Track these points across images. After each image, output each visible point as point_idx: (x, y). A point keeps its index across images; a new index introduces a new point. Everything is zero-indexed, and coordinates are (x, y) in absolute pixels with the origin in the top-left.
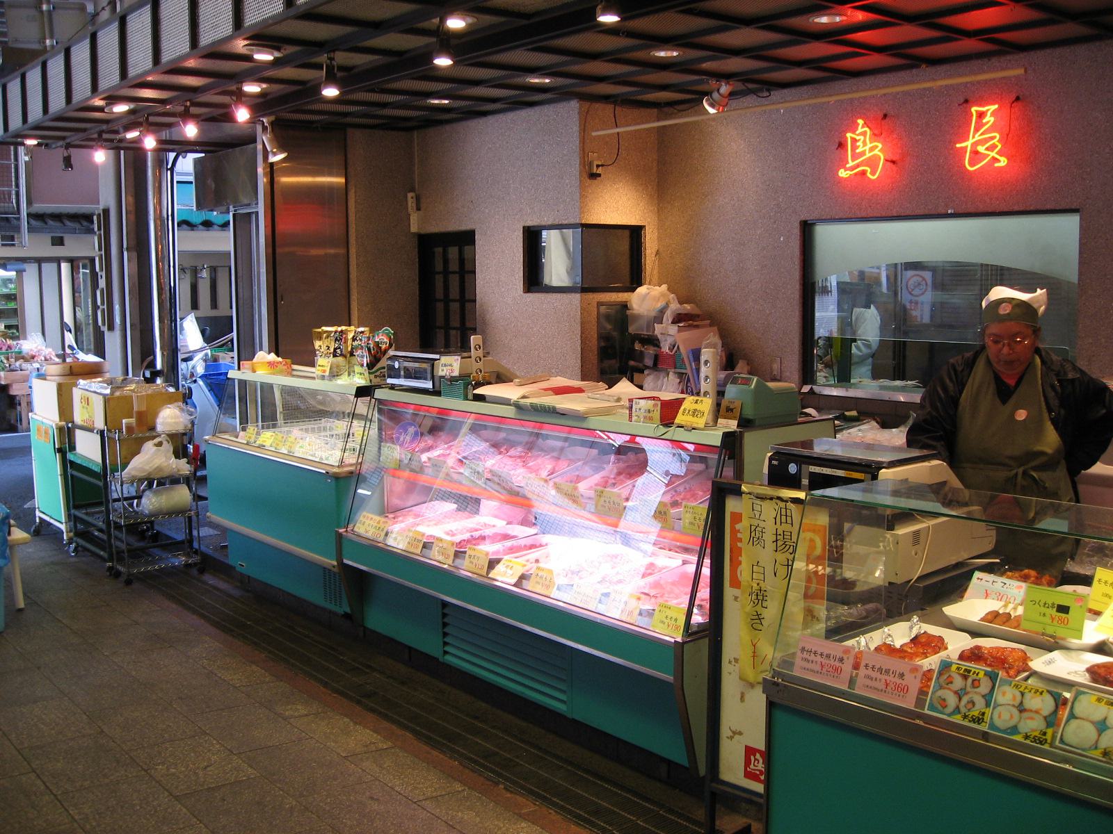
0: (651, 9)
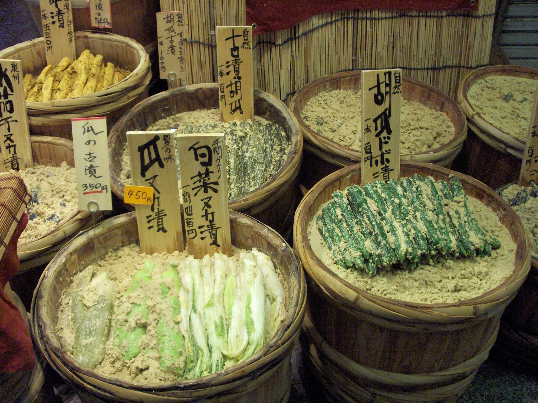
0: (60, 373)
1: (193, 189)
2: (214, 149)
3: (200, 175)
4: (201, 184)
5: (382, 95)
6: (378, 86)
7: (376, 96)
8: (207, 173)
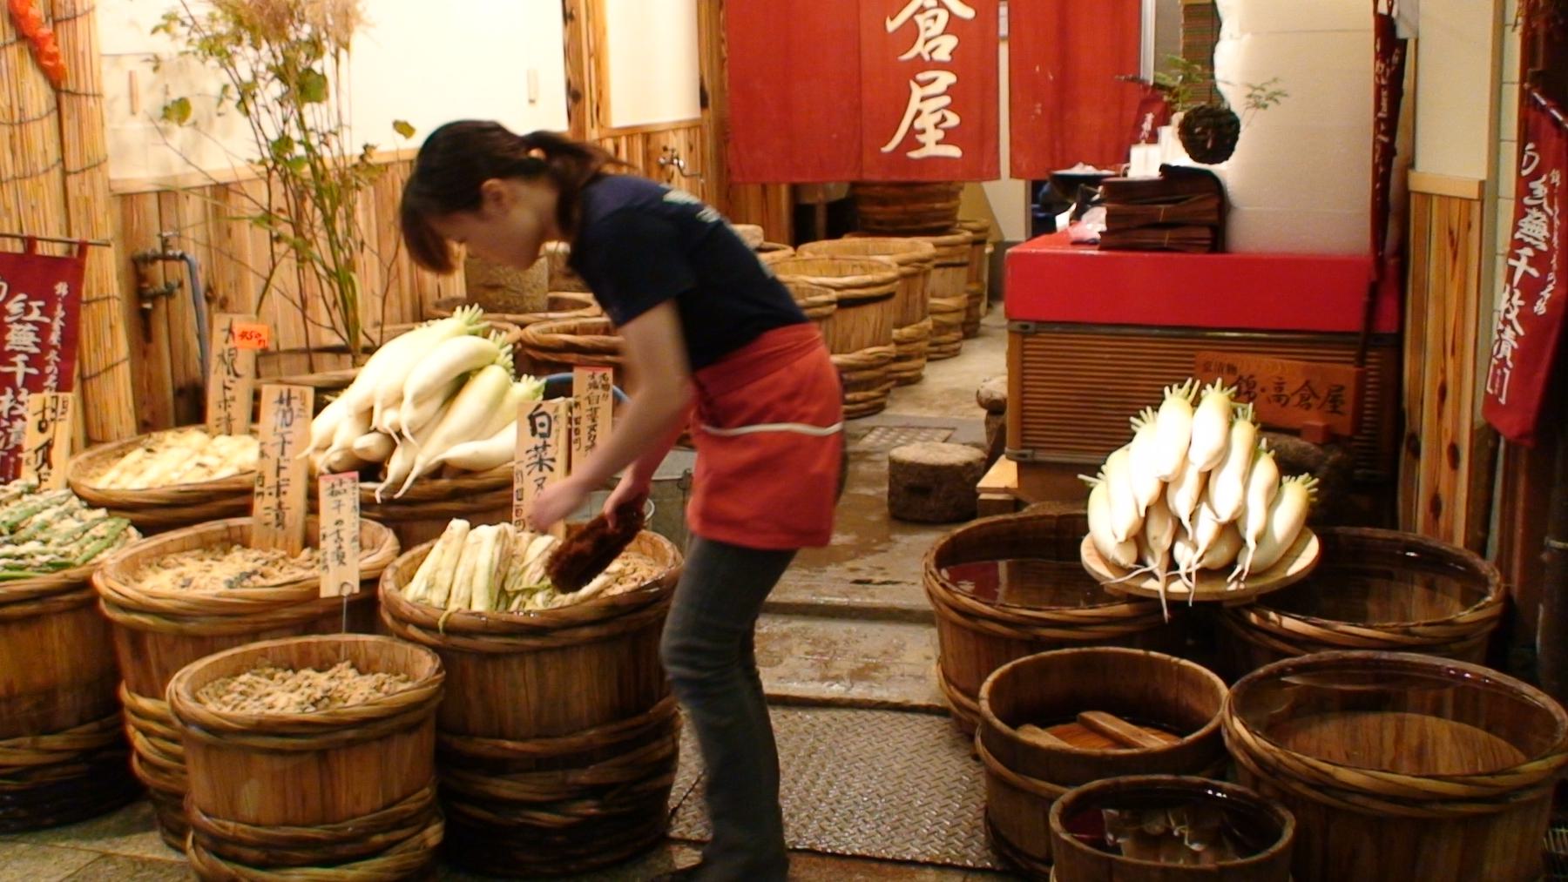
1: (528, 466)
2: (556, 417)
3: (536, 448)
4: (537, 460)
5: (46, 422)
6: (43, 411)
7: (40, 423)
8: (545, 446)
